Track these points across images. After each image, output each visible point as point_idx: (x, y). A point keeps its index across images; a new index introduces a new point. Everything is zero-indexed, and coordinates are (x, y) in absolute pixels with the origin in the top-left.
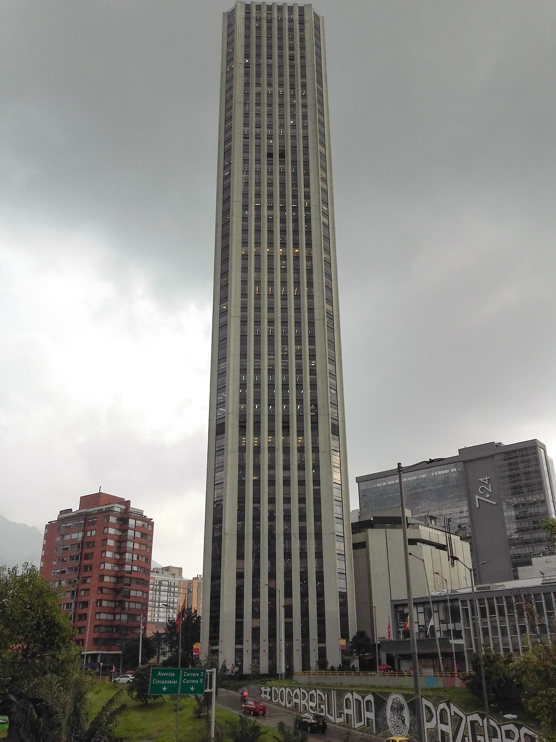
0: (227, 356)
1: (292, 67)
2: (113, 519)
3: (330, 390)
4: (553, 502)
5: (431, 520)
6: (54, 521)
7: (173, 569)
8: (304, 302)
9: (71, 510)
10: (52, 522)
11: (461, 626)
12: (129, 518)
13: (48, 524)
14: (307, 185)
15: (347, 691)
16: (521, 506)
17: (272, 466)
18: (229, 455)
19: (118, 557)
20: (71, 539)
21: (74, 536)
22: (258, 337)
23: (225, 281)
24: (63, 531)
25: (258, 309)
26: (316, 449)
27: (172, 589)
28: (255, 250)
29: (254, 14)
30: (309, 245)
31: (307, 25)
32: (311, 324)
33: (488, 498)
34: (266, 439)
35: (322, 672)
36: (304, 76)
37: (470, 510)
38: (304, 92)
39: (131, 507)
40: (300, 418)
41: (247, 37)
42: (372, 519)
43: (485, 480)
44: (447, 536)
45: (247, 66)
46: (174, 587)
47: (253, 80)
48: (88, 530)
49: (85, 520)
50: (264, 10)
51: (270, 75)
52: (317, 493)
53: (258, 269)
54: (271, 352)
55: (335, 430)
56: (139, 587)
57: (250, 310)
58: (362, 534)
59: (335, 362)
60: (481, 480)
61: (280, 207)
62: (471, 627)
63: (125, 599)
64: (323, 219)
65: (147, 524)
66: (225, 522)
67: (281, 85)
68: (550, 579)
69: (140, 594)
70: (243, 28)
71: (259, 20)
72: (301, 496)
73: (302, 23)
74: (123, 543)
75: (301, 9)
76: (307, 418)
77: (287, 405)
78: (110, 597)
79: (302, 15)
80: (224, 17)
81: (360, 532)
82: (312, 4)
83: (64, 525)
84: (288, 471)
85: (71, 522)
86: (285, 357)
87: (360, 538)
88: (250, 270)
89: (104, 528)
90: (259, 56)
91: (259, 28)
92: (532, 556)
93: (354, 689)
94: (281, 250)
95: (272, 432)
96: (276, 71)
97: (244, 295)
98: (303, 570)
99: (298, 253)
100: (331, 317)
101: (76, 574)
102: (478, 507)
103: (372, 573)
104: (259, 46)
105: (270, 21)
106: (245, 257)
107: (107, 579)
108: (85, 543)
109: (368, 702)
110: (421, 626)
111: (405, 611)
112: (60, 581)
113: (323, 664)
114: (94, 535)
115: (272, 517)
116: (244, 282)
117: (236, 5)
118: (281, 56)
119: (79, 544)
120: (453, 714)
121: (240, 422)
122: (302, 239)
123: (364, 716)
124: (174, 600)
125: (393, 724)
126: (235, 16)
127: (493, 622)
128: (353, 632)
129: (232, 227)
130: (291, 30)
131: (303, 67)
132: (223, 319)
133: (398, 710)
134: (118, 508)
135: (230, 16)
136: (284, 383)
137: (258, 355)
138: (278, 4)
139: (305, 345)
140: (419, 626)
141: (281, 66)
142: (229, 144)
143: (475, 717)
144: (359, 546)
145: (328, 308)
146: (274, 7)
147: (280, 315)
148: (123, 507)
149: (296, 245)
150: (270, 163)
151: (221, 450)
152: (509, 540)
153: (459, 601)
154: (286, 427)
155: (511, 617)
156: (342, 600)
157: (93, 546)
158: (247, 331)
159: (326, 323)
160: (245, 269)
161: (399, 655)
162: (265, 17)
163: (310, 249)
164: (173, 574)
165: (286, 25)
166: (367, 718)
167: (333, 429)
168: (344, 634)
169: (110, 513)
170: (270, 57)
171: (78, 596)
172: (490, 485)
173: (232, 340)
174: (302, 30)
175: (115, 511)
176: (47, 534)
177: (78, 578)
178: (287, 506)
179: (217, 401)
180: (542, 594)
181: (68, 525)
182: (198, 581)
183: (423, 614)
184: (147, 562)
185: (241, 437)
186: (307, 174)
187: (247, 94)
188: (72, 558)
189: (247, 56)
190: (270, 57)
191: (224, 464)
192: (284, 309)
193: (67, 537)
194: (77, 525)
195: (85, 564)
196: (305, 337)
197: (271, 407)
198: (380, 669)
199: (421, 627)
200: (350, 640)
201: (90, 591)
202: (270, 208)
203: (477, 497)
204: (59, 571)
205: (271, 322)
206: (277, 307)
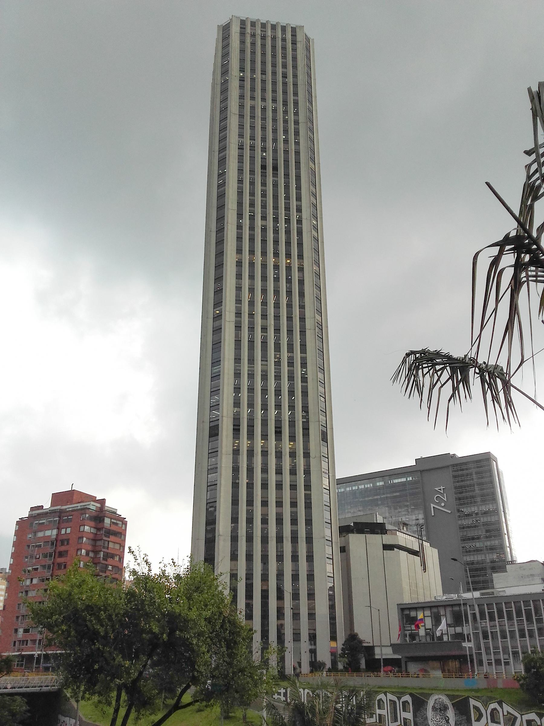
0: (222, 359)
1: (285, 84)
3: (320, 398)
4: (504, 512)
6: (26, 518)
8: (295, 311)
9: (42, 506)
10: (23, 518)
12: (105, 516)
13: (19, 520)
14: (299, 199)
15: (377, 693)
16: (474, 515)
17: (265, 470)
18: (224, 457)
20: (44, 537)
21: (48, 533)
22: (251, 342)
23: (219, 287)
24: (35, 527)
26: (307, 455)
28: (261, 259)
29: (249, 30)
30: (301, 256)
32: (303, 332)
33: (442, 507)
34: (259, 443)
35: (362, 674)
36: (296, 94)
37: (426, 518)
38: (296, 109)
39: (106, 505)
40: (292, 424)
41: (242, 51)
42: (352, 524)
44: (420, 543)
45: (242, 79)
47: (248, 94)
48: (62, 527)
49: (59, 517)
51: (264, 90)
53: (252, 277)
54: (265, 358)
55: (324, 437)
57: (244, 316)
59: (324, 370)
60: (436, 489)
61: (273, 218)
64: (314, 233)
66: (219, 524)
67: (274, 100)
71: (253, 35)
72: (264, 499)
73: (294, 43)
74: (98, 541)
75: (294, 30)
76: (298, 424)
77: (279, 411)
79: (294, 35)
80: (218, 30)
82: (303, 26)
83: (37, 522)
84: (281, 475)
85: (45, 518)
86: (278, 363)
88: (245, 276)
89: (80, 526)
90: (253, 71)
91: (253, 44)
92: (507, 563)
93: (387, 690)
95: (265, 436)
96: (269, 87)
97: (239, 301)
98: (294, 573)
99: (290, 264)
101: (49, 572)
102: (433, 515)
103: (353, 576)
104: (253, 62)
105: (263, 38)
106: (239, 264)
108: (60, 541)
109: (405, 703)
110: (428, 629)
111: (411, 614)
114: (69, 532)
115: (265, 521)
116: (239, 289)
118: (274, 73)
120: (505, 713)
121: (234, 425)
123: (400, 716)
125: (435, 724)
126: (229, 30)
129: (227, 234)
130: (284, 48)
131: (295, 85)
132: (217, 323)
133: (441, 710)
134: (93, 506)
135: (225, 30)
136: (236, 386)
137: (251, 361)
138: (261, 21)
139: (297, 354)
140: (426, 629)
141: (274, 83)
143: (532, 716)
145: (318, 319)
146: (288, 27)
147: (273, 323)
148: (99, 505)
149: (288, 255)
150: (264, 175)
151: (213, 452)
153: (468, 606)
154: (278, 432)
155: (520, 622)
157: (68, 544)
158: (241, 336)
160: (239, 276)
161: (407, 657)
162: (260, 34)
163: (301, 261)
165: (279, 43)
166: (404, 718)
167: (323, 435)
170: (264, 72)
172: (445, 494)
173: (226, 344)
174: (294, 50)
175: (91, 509)
176: (17, 530)
178: (294, 509)
179: (210, 403)
181: (41, 522)
183: (430, 617)
185: (234, 440)
186: (298, 188)
187: (242, 106)
190: (264, 72)
191: (218, 466)
192: (277, 317)
193: (40, 534)
197: (263, 411)
199: (427, 631)
202: (264, 218)
203: (432, 505)
205: (264, 329)
206: (270, 314)
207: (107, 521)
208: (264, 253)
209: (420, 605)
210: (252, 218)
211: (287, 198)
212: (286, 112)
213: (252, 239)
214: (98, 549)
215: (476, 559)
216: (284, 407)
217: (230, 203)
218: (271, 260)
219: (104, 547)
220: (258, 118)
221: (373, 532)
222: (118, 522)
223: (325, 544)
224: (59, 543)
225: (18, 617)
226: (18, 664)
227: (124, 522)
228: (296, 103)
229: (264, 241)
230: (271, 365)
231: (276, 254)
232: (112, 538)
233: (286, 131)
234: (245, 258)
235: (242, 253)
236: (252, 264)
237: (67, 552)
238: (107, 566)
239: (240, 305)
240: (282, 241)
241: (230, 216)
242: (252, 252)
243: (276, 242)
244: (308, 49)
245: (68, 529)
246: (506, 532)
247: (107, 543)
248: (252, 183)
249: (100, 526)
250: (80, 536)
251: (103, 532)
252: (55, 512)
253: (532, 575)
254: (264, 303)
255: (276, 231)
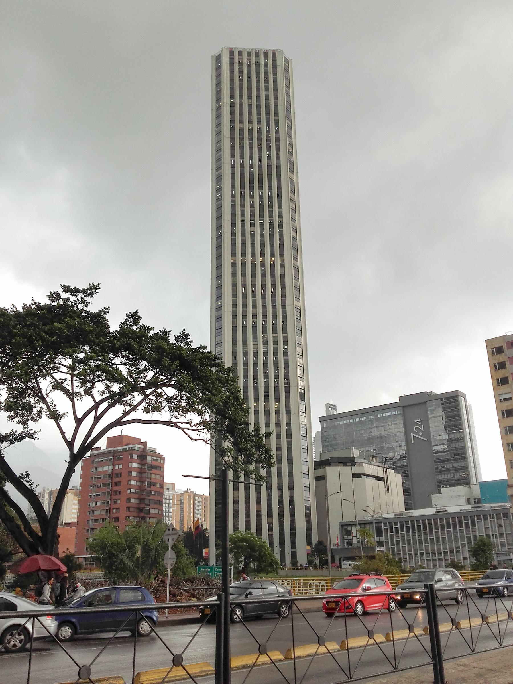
2: (135, 456)
5: (373, 458)
7: (167, 485)
9: (100, 447)
11: (383, 539)
14: (280, 206)
19: (139, 484)
20: (103, 471)
21: (105, 468)
22: (245, 328)
25: (244, 306)
26: (288, 412)
27: (168, 501)
30: (282, 255)
31: (278, 69)
32: (284, 317)
33: (421, 436)
40: (277, 389)
41: (232, 80)
43: (418, 421)
46: (169, 499)
49: (113, 456)
50: (245, 55)
52: (289, 444)
53: (244, 275)
54: (255, 339)
55: (302, 397)
56: (156, 506)
58: (322, 470)
60: (416, 421)
62: (389, 540)
63: (146, 516)
64: (291, 204)
65: (160, 459)
67: (259, 122)
68: (441, 509)
69: (157, 511)
70: (228, 72)
71: (241, 64)
78: (135, 514)
79: (274, 60)
81: (321, 468)
84: (269, 428)
86: (265, 342)
87: (320, 472)
94: (261, 259)
97: (234, 295)
100: (299, 311)
102: (413, 442)
105: (249, 65)
106: (234, 265)
107: (132, 501)
112: (96, 502)
113: (294, 563)
116: (234, 285)
117: (222, 51)
119: (110, 475)
122: (277, 250)
124: (169, 510)
127: (403, 536)
128: (315, 540)
130: (266, 73)
132: (219, 313)
135: (218, 59)
137: (245, 342)
142: (220, 171)
144: (320, 479)
148: (142, 447)
152: (436, 468)
154: (267, 396)
156: (307, 519)
157: (121, 476)
159: (296, 327)
160: (234, 275)
162: (246, 63)
164: (167, 489)
168: (309, 543)
169: (133, 452)
171: (111, 513)
174: (275, 74)
177: (110, 500)
180: (432, 520)
181: (100, 460)
182: (188, 494)
184: (161, 487)
186: (280, 197)
187: (232, 129)
188: (105, 485)
189: (232, 97)
192: (264, 306)
193: (100, 469)
194: (107, 460)
195: (115, 490)
196: (280, 327)
198: (332, 566)
200: (313, 547)
201: (120, 509)
202: (252, 225)
203: (412, 435)
204: (94, 494)
205: (255, 316)
207: (149, 458)
208: (253, 255)
209: (368, 522)
210: (243, 225)
211: (271, 206)
212: (268, 132)
213: (243, 244)
214: (143, 479)
215: (446, 477)
216: (271, 376)
217: (225, 214)
218: (259, 260)
219: (148, 478)
220: (246, 139)
221: (345, 465)
222: (157, 458)
223: (303, 477)
224: (114, 476)
225: (88, 530)
226: (90, 563)
227: (162, 458)
228: (277, 122)
229: (253, 245)
230: (260, 344)
231: (263, 255)
232: (154, 471)
233: (269, 149)
234: (238, 260)
235: (236, 256)
236: (244, 264)
237: (120, 482)
238: (151, 492)
239: (236, 298)
240: (267, 244)
241: (225, 226)
242: (243, 254)
243: (262, 245)
244: (287, 71)
245: (120, 465)
246: (471, 455)
247: (149, 474)
248: (243, 197)
249: (143, 462)
250: (129, 470)
251: (146, 467)
252: (110, 453)
253: (459, 496)
254: (254, 295)
255: (262, 235)
